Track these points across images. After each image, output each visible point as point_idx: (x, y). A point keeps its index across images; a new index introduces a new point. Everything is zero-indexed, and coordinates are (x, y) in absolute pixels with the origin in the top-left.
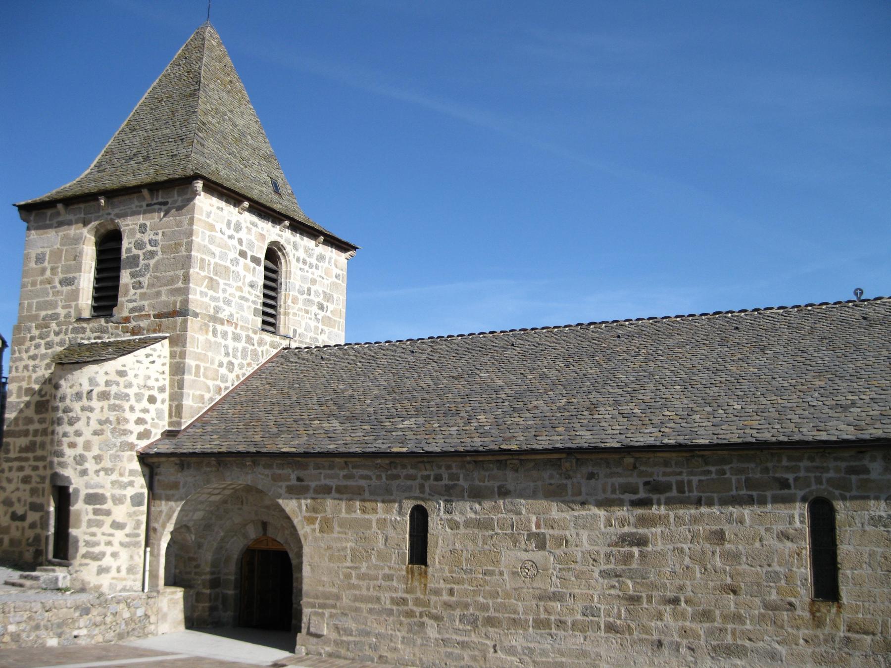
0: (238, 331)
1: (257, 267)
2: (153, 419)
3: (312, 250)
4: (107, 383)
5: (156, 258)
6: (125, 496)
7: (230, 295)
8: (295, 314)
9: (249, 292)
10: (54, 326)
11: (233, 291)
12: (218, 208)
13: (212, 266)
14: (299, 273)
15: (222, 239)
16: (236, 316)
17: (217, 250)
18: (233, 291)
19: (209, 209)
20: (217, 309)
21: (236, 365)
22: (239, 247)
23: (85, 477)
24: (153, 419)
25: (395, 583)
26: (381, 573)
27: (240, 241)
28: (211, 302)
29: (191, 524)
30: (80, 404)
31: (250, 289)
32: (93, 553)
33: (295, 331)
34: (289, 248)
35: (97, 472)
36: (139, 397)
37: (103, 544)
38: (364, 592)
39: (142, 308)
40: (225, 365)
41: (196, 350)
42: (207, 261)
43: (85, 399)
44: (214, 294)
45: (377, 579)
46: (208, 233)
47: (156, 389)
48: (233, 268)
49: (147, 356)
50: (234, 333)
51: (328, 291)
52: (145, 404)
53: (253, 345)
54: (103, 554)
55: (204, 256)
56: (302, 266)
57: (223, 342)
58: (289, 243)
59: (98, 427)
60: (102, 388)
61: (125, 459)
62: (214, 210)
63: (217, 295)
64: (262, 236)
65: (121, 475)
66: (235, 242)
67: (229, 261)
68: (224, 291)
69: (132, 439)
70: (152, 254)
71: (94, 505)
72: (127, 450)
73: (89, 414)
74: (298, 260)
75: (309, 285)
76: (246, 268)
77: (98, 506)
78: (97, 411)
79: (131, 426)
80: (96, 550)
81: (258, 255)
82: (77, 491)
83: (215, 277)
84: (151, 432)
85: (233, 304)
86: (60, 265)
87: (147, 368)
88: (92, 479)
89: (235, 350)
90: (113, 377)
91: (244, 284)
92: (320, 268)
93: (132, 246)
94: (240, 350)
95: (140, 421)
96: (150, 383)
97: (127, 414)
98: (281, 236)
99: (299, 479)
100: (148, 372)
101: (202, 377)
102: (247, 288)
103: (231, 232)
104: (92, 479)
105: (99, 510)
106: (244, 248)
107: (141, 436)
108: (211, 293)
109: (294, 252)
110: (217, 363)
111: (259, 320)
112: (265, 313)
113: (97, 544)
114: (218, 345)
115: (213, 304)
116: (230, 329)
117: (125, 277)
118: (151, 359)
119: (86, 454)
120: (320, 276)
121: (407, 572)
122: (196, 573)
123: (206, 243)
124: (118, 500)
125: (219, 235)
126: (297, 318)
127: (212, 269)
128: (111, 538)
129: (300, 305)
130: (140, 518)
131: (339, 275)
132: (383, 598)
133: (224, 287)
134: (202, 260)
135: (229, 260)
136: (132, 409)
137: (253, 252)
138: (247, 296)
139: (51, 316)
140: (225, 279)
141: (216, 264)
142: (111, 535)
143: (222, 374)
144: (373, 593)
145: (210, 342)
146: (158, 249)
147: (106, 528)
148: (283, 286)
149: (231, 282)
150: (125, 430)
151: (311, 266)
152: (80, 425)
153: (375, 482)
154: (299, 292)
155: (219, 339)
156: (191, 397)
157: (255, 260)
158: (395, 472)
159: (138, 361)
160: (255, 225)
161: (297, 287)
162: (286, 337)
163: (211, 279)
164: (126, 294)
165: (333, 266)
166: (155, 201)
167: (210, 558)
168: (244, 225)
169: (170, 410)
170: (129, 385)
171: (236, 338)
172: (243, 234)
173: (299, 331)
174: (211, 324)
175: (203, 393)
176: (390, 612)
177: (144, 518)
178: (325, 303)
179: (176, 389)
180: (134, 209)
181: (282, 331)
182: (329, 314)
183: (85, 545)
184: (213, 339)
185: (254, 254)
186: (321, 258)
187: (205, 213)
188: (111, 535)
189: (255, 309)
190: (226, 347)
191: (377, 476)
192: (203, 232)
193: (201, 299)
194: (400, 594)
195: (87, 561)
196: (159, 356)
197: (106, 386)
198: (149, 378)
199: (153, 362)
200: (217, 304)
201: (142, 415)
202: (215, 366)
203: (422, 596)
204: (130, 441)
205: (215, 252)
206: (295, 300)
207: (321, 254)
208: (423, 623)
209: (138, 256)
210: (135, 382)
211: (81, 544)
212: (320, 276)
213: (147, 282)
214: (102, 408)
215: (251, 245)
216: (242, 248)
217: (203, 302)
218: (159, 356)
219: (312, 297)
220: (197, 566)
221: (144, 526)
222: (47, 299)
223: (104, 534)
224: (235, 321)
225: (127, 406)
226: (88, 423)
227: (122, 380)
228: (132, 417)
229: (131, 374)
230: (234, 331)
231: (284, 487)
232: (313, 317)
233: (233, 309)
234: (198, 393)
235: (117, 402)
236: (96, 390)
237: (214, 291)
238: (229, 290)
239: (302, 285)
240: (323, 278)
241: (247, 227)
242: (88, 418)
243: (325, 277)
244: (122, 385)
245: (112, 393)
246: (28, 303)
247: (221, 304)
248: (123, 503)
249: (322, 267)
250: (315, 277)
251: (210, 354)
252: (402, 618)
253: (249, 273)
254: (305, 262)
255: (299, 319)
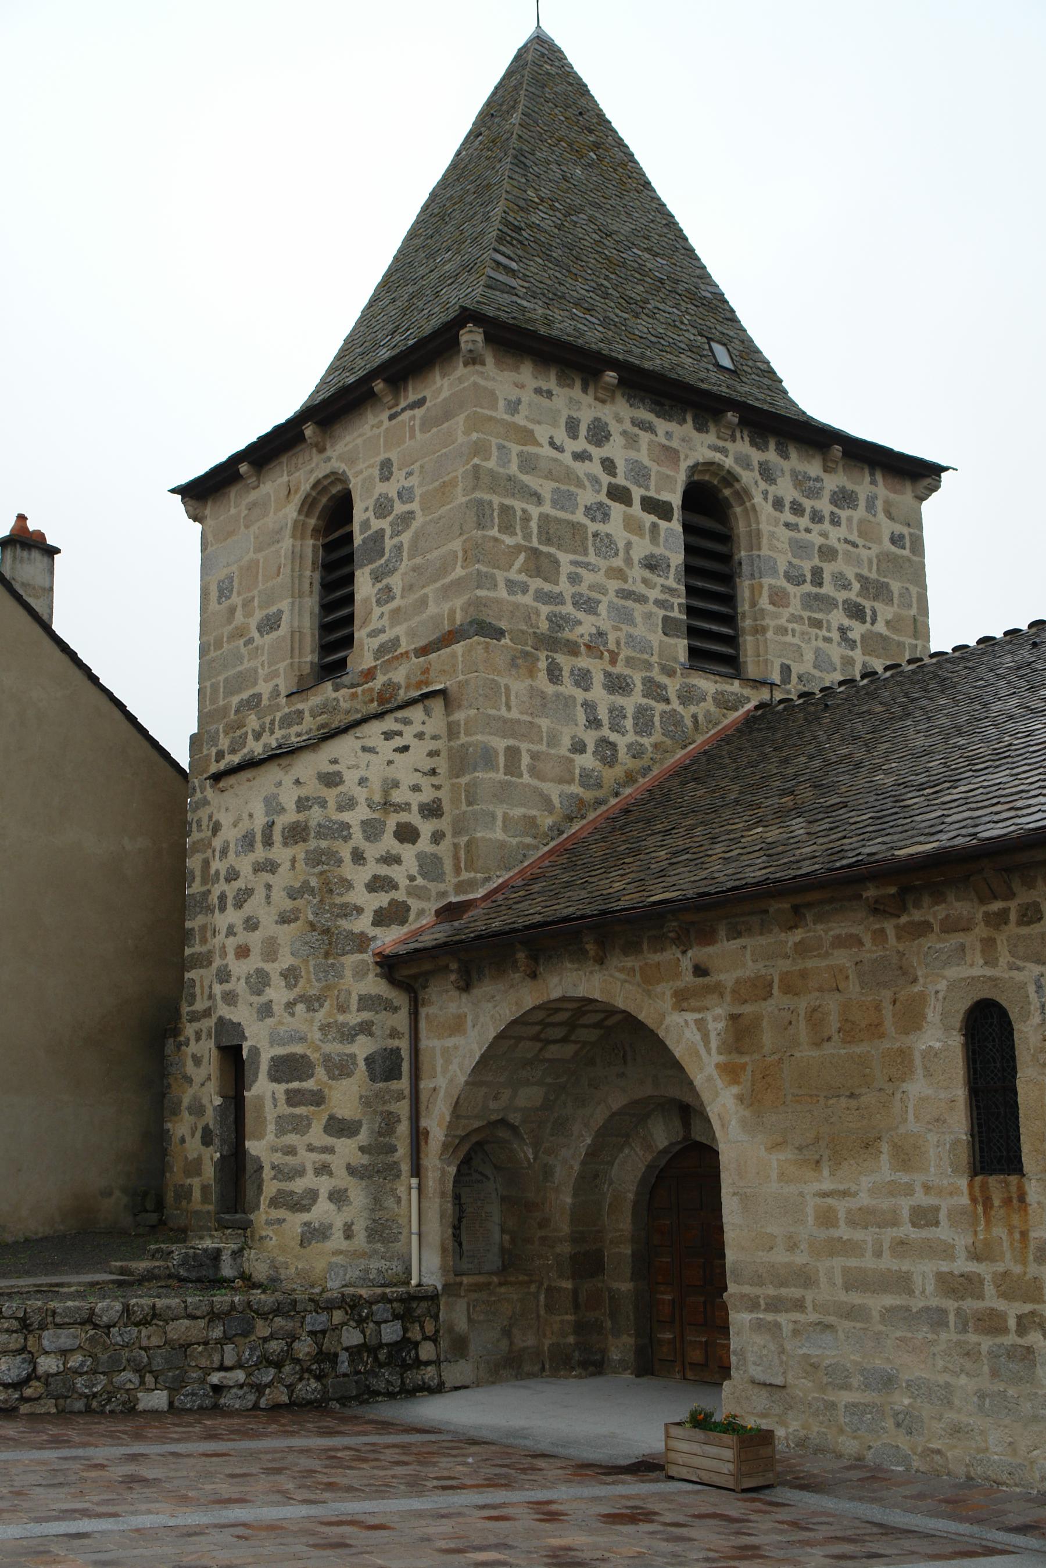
0: (620, 669)
1: (663, 524)
2: (412, 879)
3: (818, 479)
4: (302, 804)
5: (415, 525)
6: (353, 1056)
7: (591, 587)
8: (783, 631)
9: (645, 581)
10: (253, 722)
11: (599, 578)
12: (538, 391)
13: (534, 525)
14: (785, 534)
15: (556, 460)
16: (611, 638)
17: (546, 488)
18: (599, 578)
19: (514, 394)
20: (558, 622)
21: (622, 751)
22: (605, 479)
23: (269, 1021)
24: (412, 879)
25: (943, 1232)
26: (905, 1205)
27: (609, 466)
28: (540, 606)
29: (515, 1118)
30: (252, 857)
31: (647, 574)
32: (292, 1193)
33: (786, 670)
34: (748, 477)
35: (290, 1005)
36: (372, 830)
37: (310, 1172)
38: (869, 1262)
39: (395, 642)
40: (591, 748)
41: (503, 712)
42: (519, 513)
43: (259, 845)
44: (547, 587)
45: (895, 1223)
46: (515, 449)
47: (415, 808)
48: (592, 527)
49: (388, 736)
50: (608, 675)
51: (873, 575)
52: (389, 843)
53: (667, 701)
54: (313, 1195)
55: (508, 502)
56: (792, 519)
57: (580, 695)
58: (748, 466)
59: (288, 904)
60: (291, 816)
61: (348, 973)
62: (527, 396)
63: (556, 589)
64: (671, 455)
65: (343, 1009)
66: (595, 468)
67: (581, 509)
68: (574, 579)
69: (363, 924)
70: (407, 518)
71: (287, 1082)
72: (351, 952)
73: (267, 877)
74: (778, 504)
75: (816, 562)
76: (632, 525)
77: (295, 1085)
78: (284, 868)
79: (359, 896)
80: (299, 1185)
81: (664, 496)
82: (255, 1051)
83: (544, 549)
84: (408, 909)
85: (602, 609)
86: (256, 592)
87: (390, 762)
88: (281, 1023)
89: (617, 714)
90: (313, 788)
91: (628, 561)
92: (844, 522)
93: (370, 514)
94: (630, 711)
95: (377, 884)
96: (398, 796)
97: (349, 870)
98: (724, 451)
99: (700, 971)
100: (391, 772)
101: (526, 775)
102: (637, 572)
103: (581, 444)
104: (281, 1023)
105: (297, 1091)
106: (620, 480)
107: (382, 918)
108: (536, 583)
109: (763, 485)
110: (566, 742)
111: (680, 646)
112: (692, 632)
113: (300, 1172)
114: (568, 702)
115: (545, 610)
116: (597, 668)
117: (364, 586)
118: (398, 742)
119: (268, 967)
120: (846, 541)
121: (974, 1199)
122: (543, 1239)
123: (514, 468)
124: (341, 1068)
125: (547, 451)
126: (789, 638)
127: (535, 531)
128: (326, 1157)
129: (795, 606)
130: (393, 1107)
131: (902, 537)
132: (917, 1279)
133: (573, 569)
134: (505, 510)
135: (582, 509)
136: (358, 857)
137: (647, 488)
138: (641, 589)
139: (248, 701)
140: (575, 552)
141: (544, 518)
142: (329, 1150)
143: (584, 769)
144: (888, 1263)
145: (543, 695)
146: (415, 506)
147: (317, 1135)
148: (745, 568)
149: (592, 558)
150: (345, 905)
151: (817, 517)
152: (254, 906)
153: (870, 951)
154: (788, 577)
155: (568, 688)
156: (499, 822)
157: (656, 507)
158: (917, 915)
159: (364, 749)
160: (649, 428)
161: (782, 568)
162: (759, 683)
163: (535, 551)
164: (365, 622)
165: (881, 516)
166: (403, 404)
167: (569, 1200)
168: (614, 428)
169: (456, 858)
170: (348, 804)
171: (617, 685)
172: (615, 449)
173: (796, 669)
174: (542, 655)
175: (534, 812)
176: (937, 1319)
177: (403, 1108)
178: (867, 604)
179: (464, 807)
180: (369, 434)
181: (752, 671)
182: (880, 627)
183: (275, 1178)
184: (550, 689)
185: (652, 493)
186: (844, 498)
187: (501, 404)
188: (329, 1150)
189: (665, 619)
190: (589, 706)
191: (875, 932)
192: (501, 447)
193: (512, 598)
194: (963, 1265)
195: (281, 1213)
196: (420, 736)
197: (299, 812)
198: (396, 785)
199: (405, 749)
200: (557, 609)
201: (383, 870)
202: (564, 751)
203: (1017, 1269)
204: (356, 931)
205: (540, 490)
206: (779, 598)
207: (843, 490)
208: (1029, 1349)
209: (381, 533)
210: (361, 794)
211: (267, 1173)
212: (846, 541)
213: (400, 582)
214: (293, 861)
215: (640, 474)
216: (613, 480)
217: (517, 606)
218: (420, 736)
219: (828, 589)
220: (544, 1224)
221: (403, 1128)
222: (240, 668)
223: (311, 1148)
224: (612, 646)
225: (345, 852)
226: (268, 897)
227: (331, 795)
228: (361, 876)
229: (351, 777)
230: (610, 668)
231: (668, 994)
232: (835, 635)
233: (604, 620)
234: (518, 812)
235: (324, 844)
236: (282, 821)
237: (546, 579)
238: (588, 577)
239: (795, 561)
240: (855, 545)
241: (624, 433)
242: (269, 887)
243: (860, 542)
244: (332, 804)
245: (313, 824)
246: (212, 685)
247: (568, 609)
248: (349, 1075)
249: (850, 519)
250: (833, 542)
251: (544, 723)
252: (973, 1338)
253: (642, 536)
254: (797, 509)
255: (796, 641)
